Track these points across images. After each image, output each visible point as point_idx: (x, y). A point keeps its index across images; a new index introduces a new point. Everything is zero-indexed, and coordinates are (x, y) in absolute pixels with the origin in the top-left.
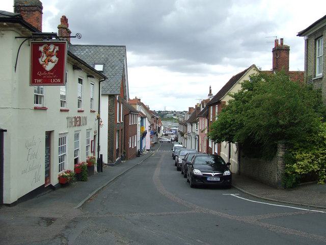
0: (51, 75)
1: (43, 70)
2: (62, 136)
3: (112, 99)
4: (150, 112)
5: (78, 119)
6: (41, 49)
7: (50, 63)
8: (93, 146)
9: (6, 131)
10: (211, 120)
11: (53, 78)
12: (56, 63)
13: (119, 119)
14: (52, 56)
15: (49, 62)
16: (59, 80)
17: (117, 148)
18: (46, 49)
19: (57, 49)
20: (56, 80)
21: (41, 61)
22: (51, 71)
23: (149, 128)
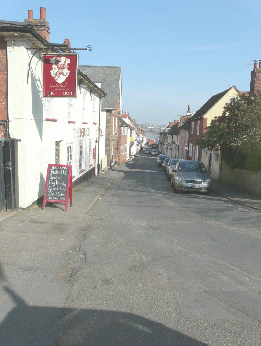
0: (63, 88)
1: (55, 83)
2: (70, 145)
3: (109, 113)
4: (137, 125)
5: (83, 130)
6: (53, 59)
7: (62, 75)
8: (94, 153)
9: (20, 140)
10: (192, 133)
11: (64, 91)
12: (67, 76)
13: (114, 131)
14: (64, 68)
15: (60, 74)
16: (70, 93)
17: (112, 155)
18: (57, 62)
19: (68, 61)
20: (68, 93)
21: (53, 73)
22: (63, 84)
23: (136, 138)
